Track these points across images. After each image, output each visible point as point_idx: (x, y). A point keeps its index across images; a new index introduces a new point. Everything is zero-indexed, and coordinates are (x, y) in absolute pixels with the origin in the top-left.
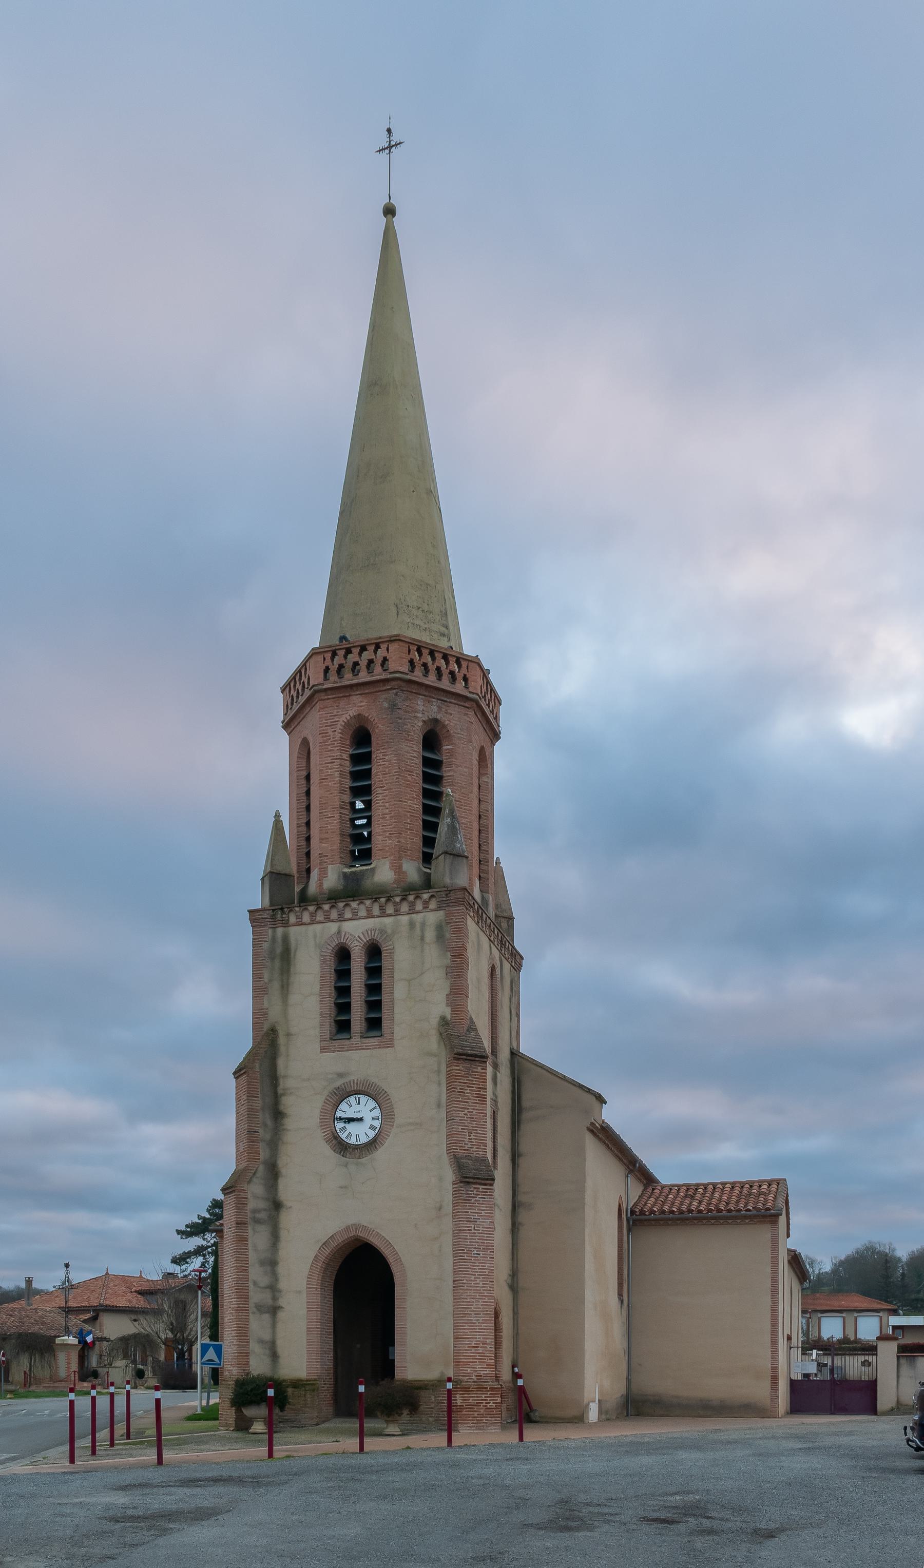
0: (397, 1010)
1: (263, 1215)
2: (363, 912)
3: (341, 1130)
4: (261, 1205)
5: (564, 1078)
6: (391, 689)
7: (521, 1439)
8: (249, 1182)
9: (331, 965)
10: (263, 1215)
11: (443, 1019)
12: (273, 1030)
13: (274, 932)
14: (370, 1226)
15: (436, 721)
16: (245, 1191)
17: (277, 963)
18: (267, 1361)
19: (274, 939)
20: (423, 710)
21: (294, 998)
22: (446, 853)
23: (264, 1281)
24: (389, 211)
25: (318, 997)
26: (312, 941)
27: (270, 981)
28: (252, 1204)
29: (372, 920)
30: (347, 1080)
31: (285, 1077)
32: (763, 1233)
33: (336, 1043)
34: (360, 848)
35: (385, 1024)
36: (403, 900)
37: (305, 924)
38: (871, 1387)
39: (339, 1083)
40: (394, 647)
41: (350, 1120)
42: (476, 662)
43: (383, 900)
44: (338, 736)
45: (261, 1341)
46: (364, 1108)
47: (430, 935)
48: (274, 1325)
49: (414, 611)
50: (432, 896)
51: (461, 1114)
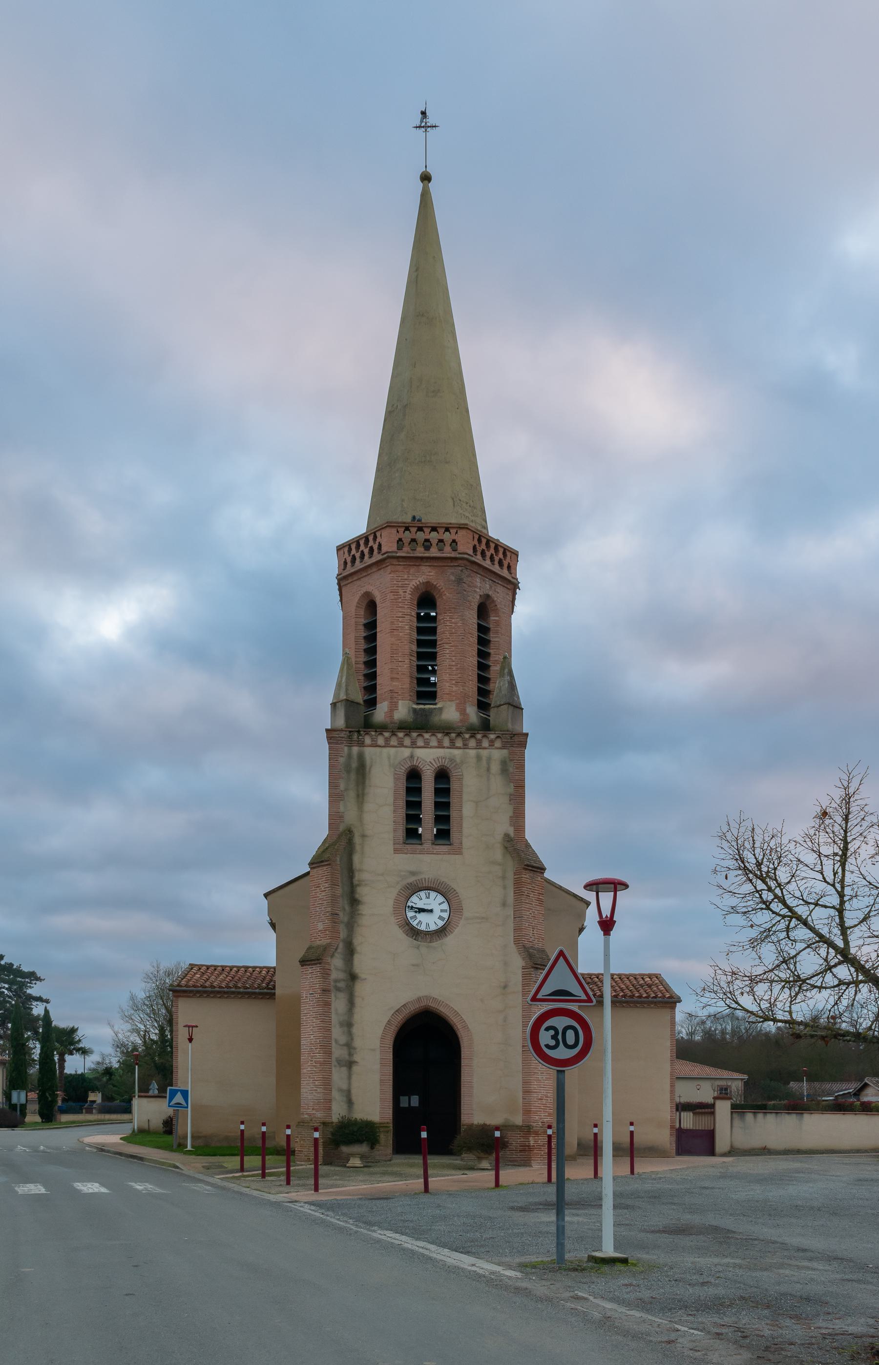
0: (465, 824)
1: (341, 985)
2: (434, 743)
3: (411, 918)
4: (341, 975)
5: (560, 888)
7: (632, 1172)
8: (332, 956)
9: (403, 784)
10: (341, 985)
11: (507, 835)
12: (349, 832)
14: (440, 999)
15: (488, 596)
16: (329, 964)
17: (353, 776)
18: (345, 1106)
19: (350, 756)
20: (480, 586)
21: (368, 806)
22: (509, 704)
23: (343, 1039)
24: (426, 178)
25: (392, 808)
26: (386, 762)
27: (346, 790)
28: (335, 975)
30: (419, 877)
31: (360, 870)
32: (665, 1014)
34: (426, 692)
35: (454, 834)
36: (471, 737)
37: (380, 746)
38: (710, 1135)
39: (412, 879)
40: (462, 533)
41: (421, 910)
43: (453, 735)
44: (408, 597)
45: (340, 1090)
46: (435, 902)
47: (495, 767)
48: (350, 1077)
49: (464, 505)
50: (498, 737)
51: (528, 913)
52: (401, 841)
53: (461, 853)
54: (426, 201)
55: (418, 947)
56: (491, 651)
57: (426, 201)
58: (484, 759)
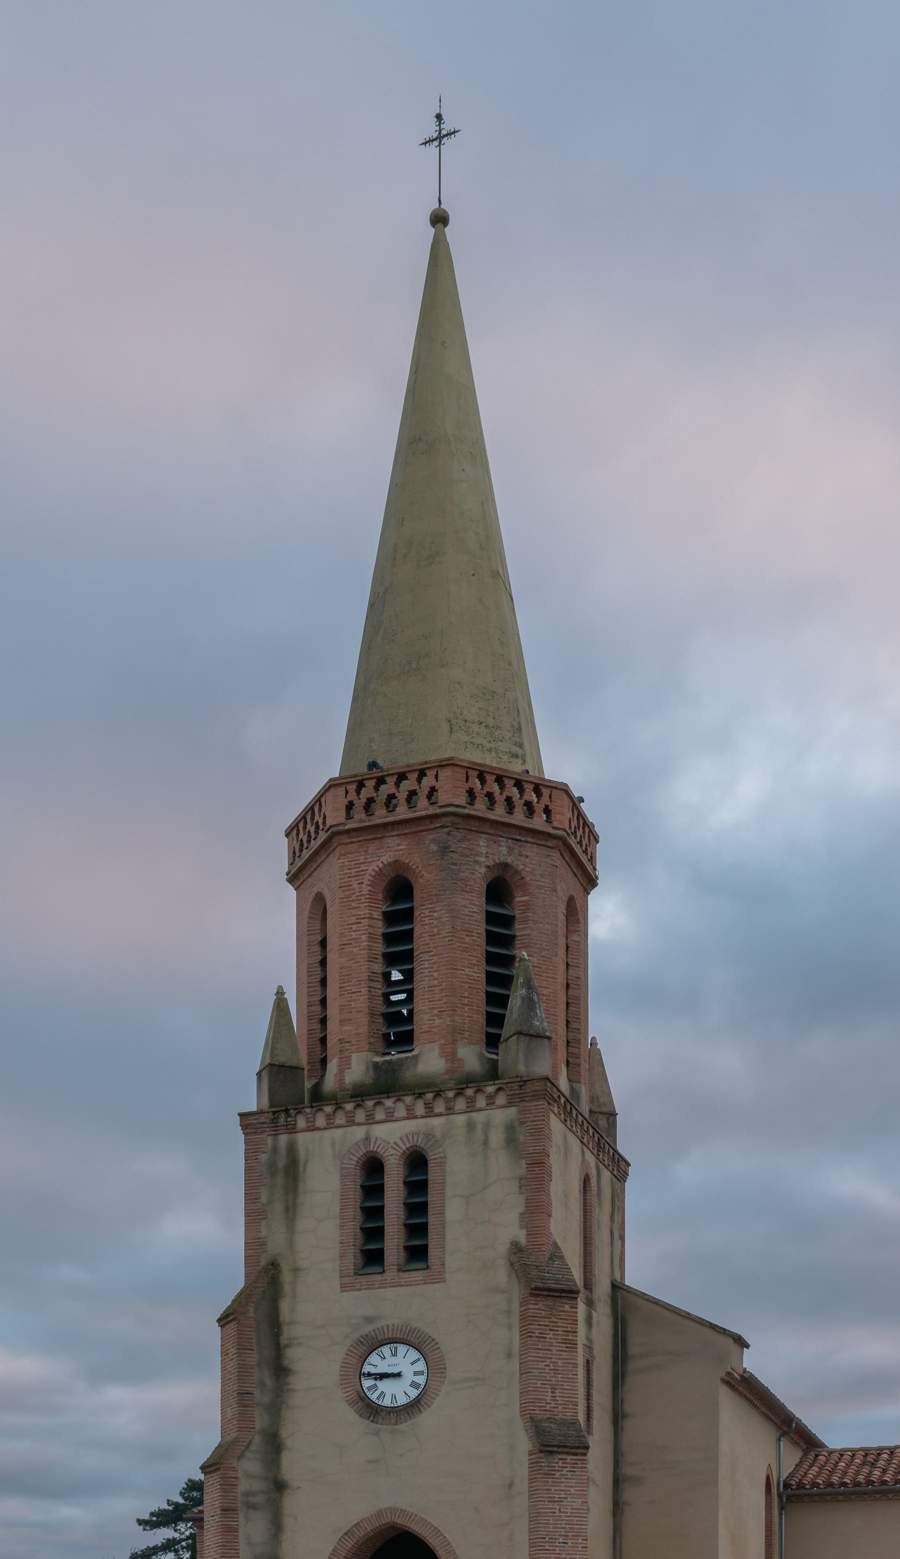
0: (450, 1235)
1: (259, 1499)
2: (401, 1111)
3: (369, 1388)
6: (442, 827)
8: (240, 1457)
9: (356, 1180)
10: (259, 1499)
12: (274, 1265)
13: (275, 1141)
15: (506, 866)
16: (234, 1469)
17: (280, 1180)
19: (275, 1150)
20: (487, 853)
21: (304, 1223)
22: (519, 1033)
24: (439, 219)
26: (328, 1153)
27: (270, 1202)
29: (413, 1122)
30: (378, 1325)
33: (363, 1279)
34: (397, 1029)
35: (432, 1252)
37: (319, 1129)
39: (367, 1329)
40: (444, 774)
42: (564, 789)
43: (430, 1096)
44: (366, 889)
46: (405, 1361)
47: (497, 1137)
49: (475, 727)
50: (500, 1089)
51: (542, 1365)
52: (352, 1271)
53: (443, 1281)
54: (439, 261)
55: (377, 1434)
56: (516, 952)
57: (439, 261)
58: (479, 1127)
